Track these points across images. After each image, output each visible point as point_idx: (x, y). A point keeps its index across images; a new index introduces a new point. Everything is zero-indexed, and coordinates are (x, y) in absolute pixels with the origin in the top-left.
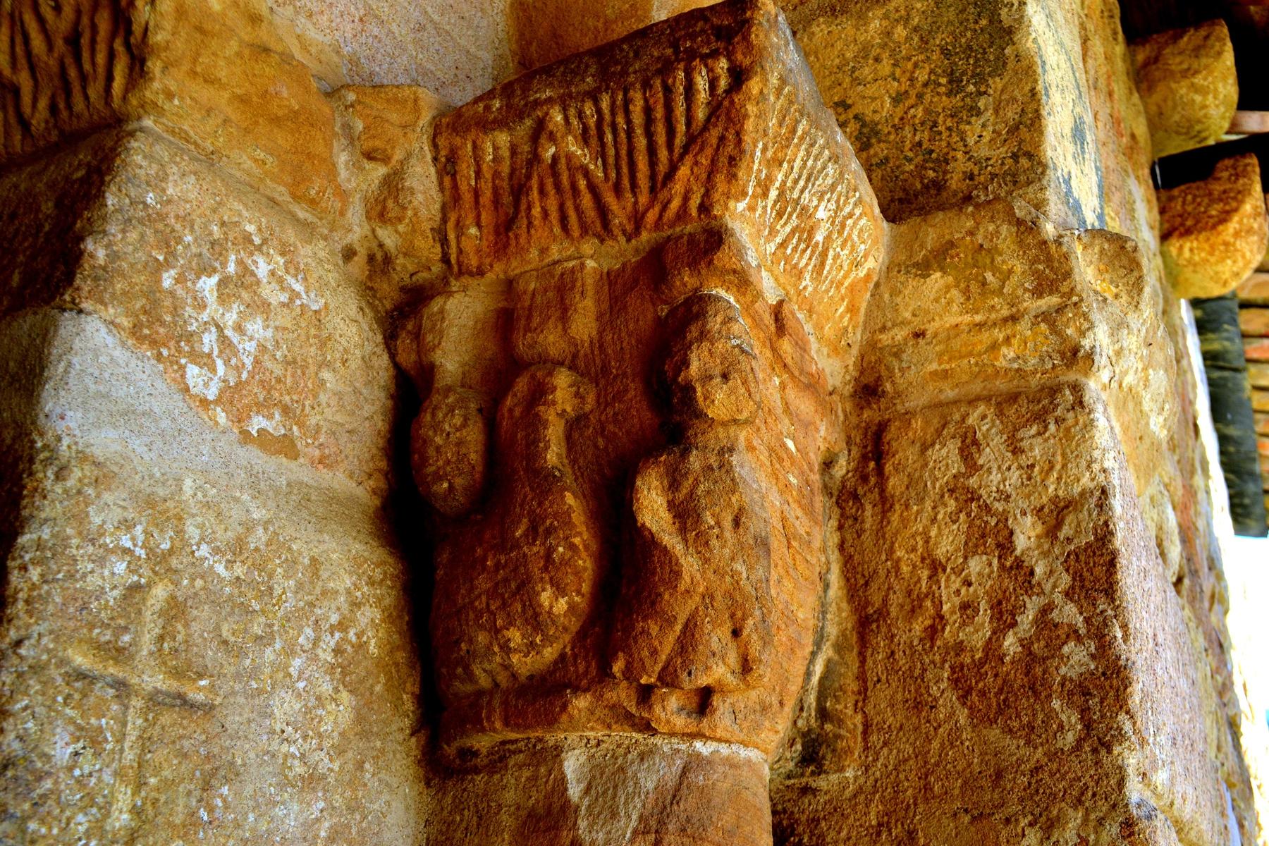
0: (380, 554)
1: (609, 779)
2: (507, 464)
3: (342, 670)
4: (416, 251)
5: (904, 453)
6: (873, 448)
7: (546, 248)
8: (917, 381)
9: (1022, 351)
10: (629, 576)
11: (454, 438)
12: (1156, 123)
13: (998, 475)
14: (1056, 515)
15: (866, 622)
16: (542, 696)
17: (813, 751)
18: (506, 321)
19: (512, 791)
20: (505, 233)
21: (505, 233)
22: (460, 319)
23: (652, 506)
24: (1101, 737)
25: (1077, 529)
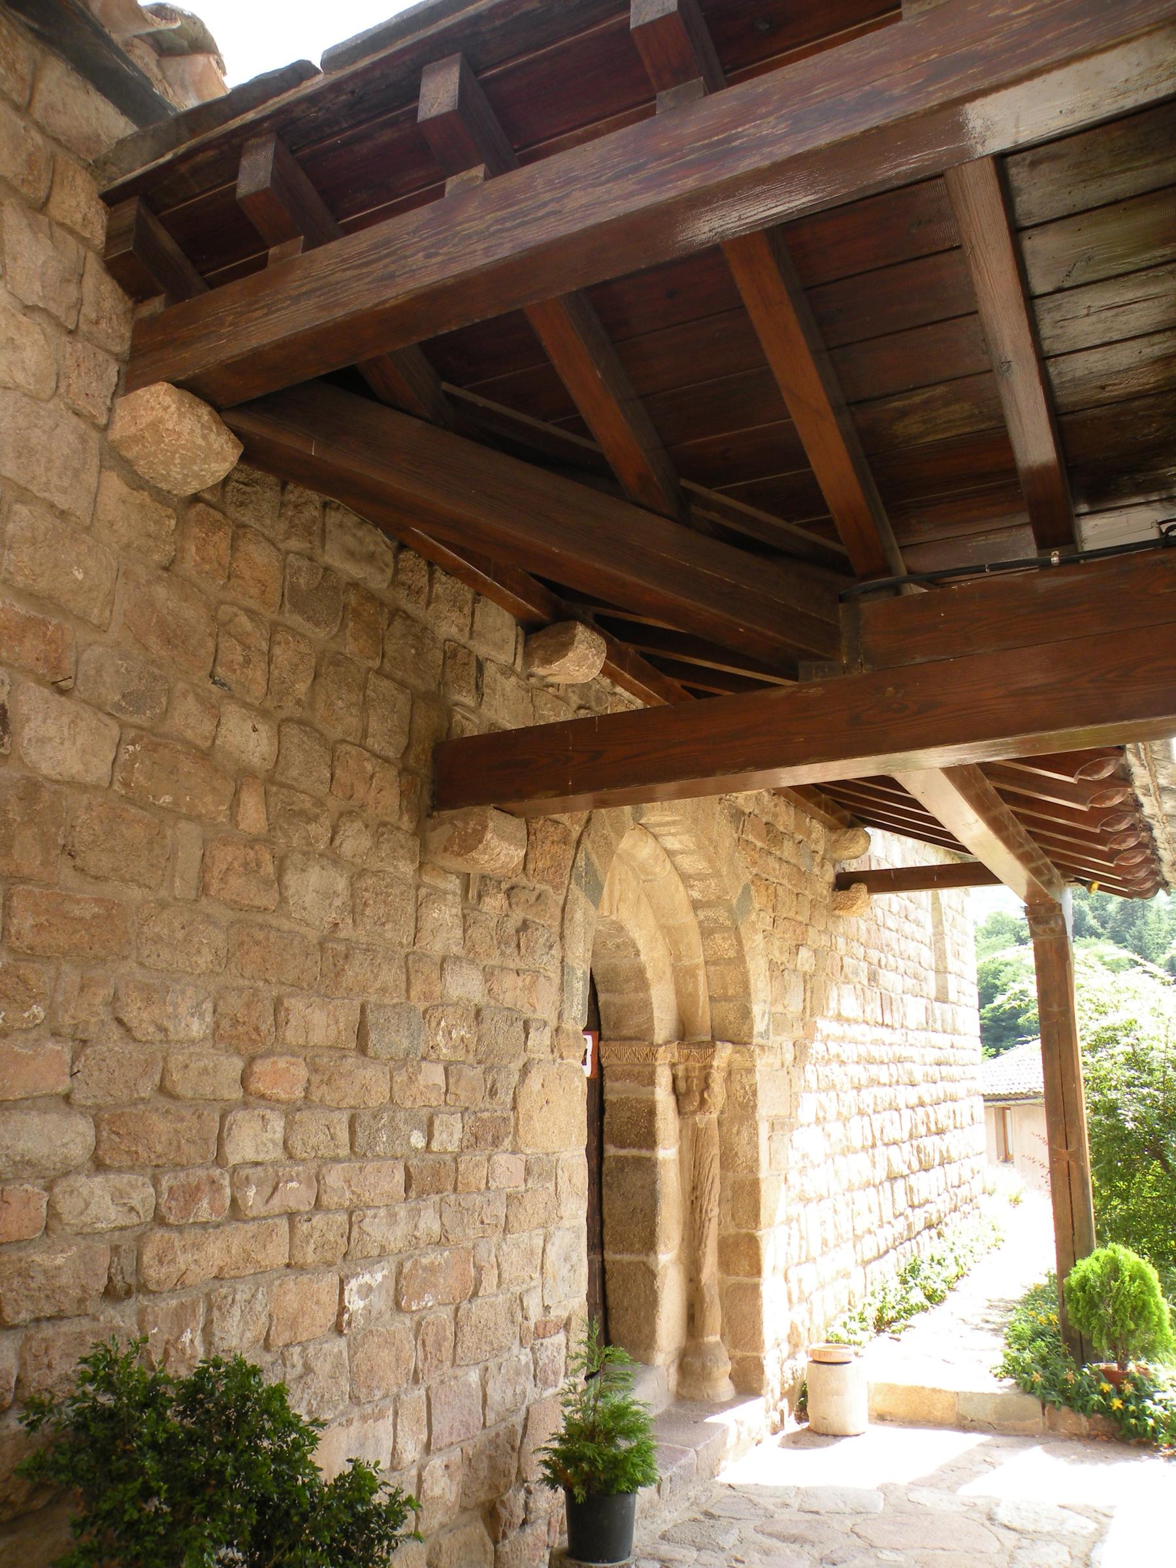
0: (595, 636)
1: (701, 1120)
2: (689, 1091)
4: (675, 1060)
5: (733, 1076)
6: (730, 1074)
7: (691, 1063)
8: (735, 1066)
9: (748, 1064)
10: (703, 1102)
11: (682, 1085)
12: (679, 74)
13: (745, 1080)
14: (751, 1086)
15: (728, 1097)
16: (694, 1113)
17: (722, 1112)
18: (687, 1070)
19: (690, 1121)
20: (687, 1060)
21: (687, 1060)
22: (681, 1068)
23: (706, 1095)
24: (754, 1112)
25: (753, 1088)
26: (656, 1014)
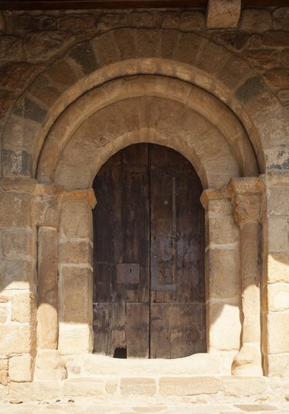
3: (231, 224)
26: (207, 173)
